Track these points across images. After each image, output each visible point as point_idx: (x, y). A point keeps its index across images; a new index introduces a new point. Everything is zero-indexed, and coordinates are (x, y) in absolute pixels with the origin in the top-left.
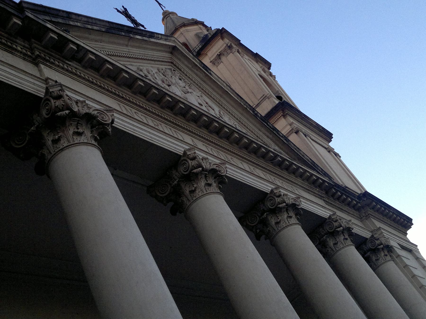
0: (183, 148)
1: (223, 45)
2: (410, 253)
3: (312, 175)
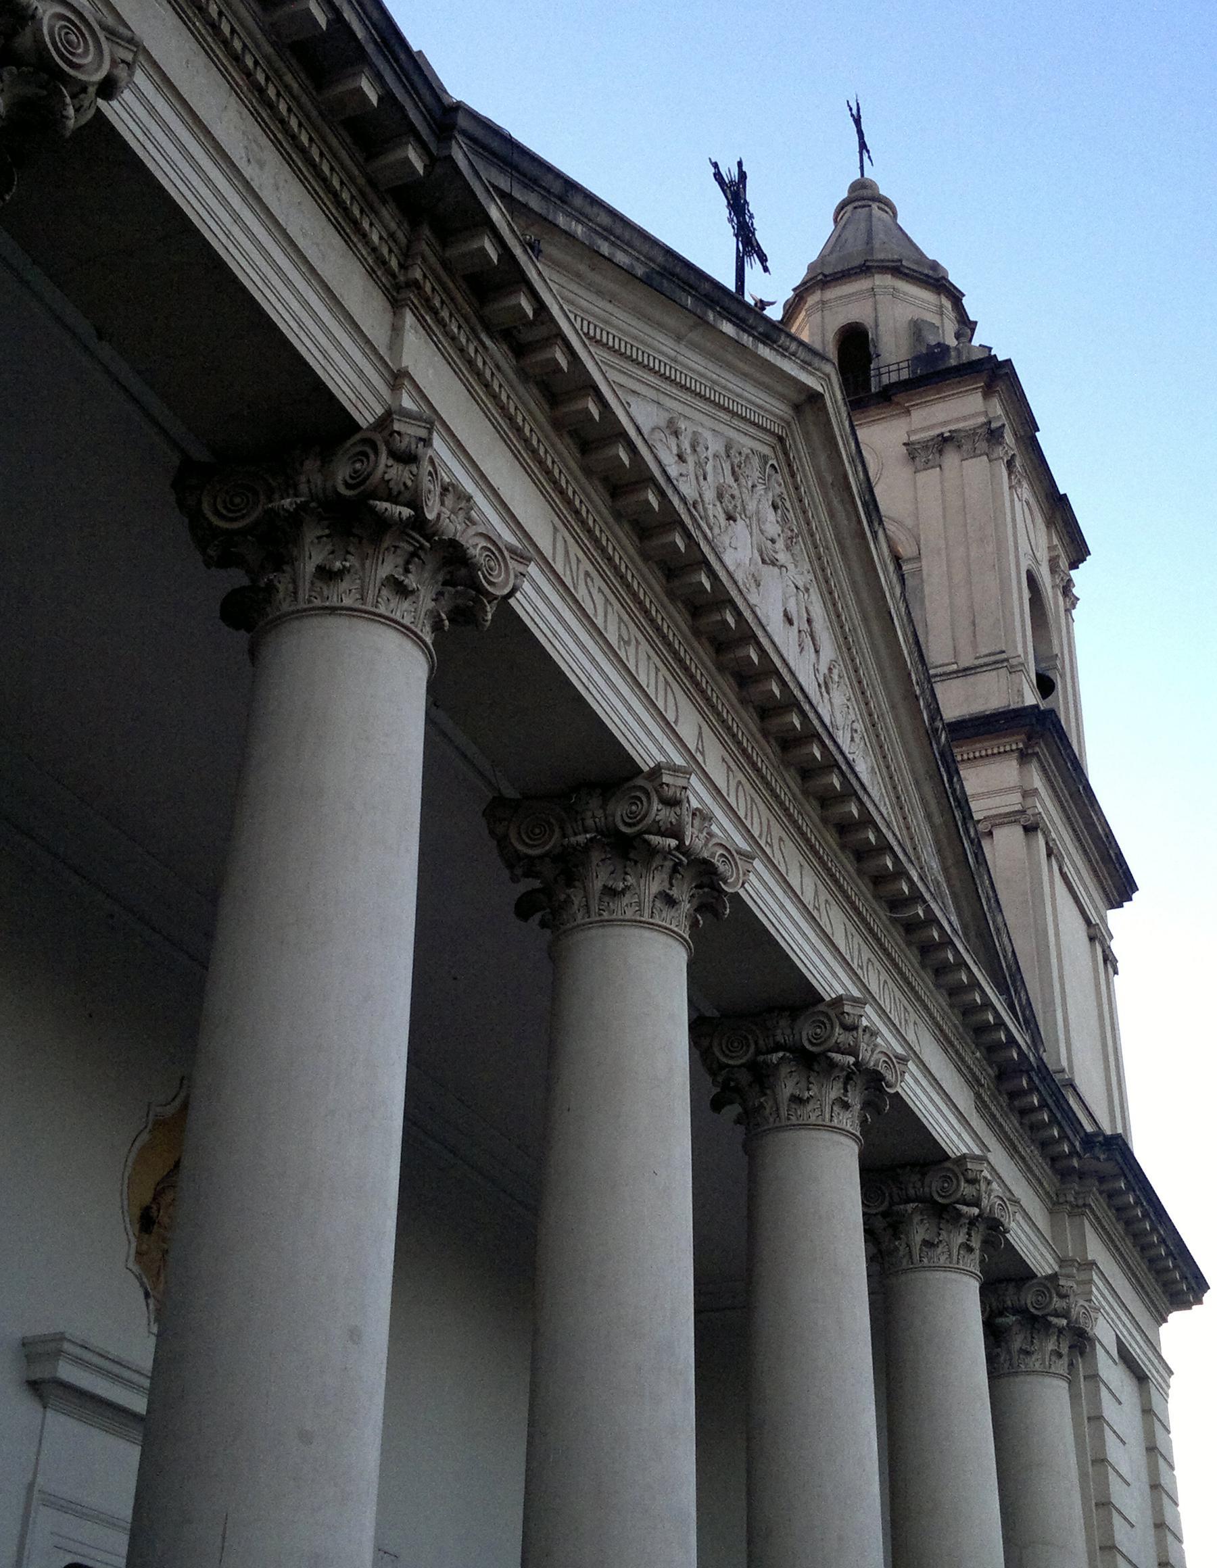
0: (661, 749)
1: (974, 416)
2: (1135, 1381)
3: (988, 1005)
